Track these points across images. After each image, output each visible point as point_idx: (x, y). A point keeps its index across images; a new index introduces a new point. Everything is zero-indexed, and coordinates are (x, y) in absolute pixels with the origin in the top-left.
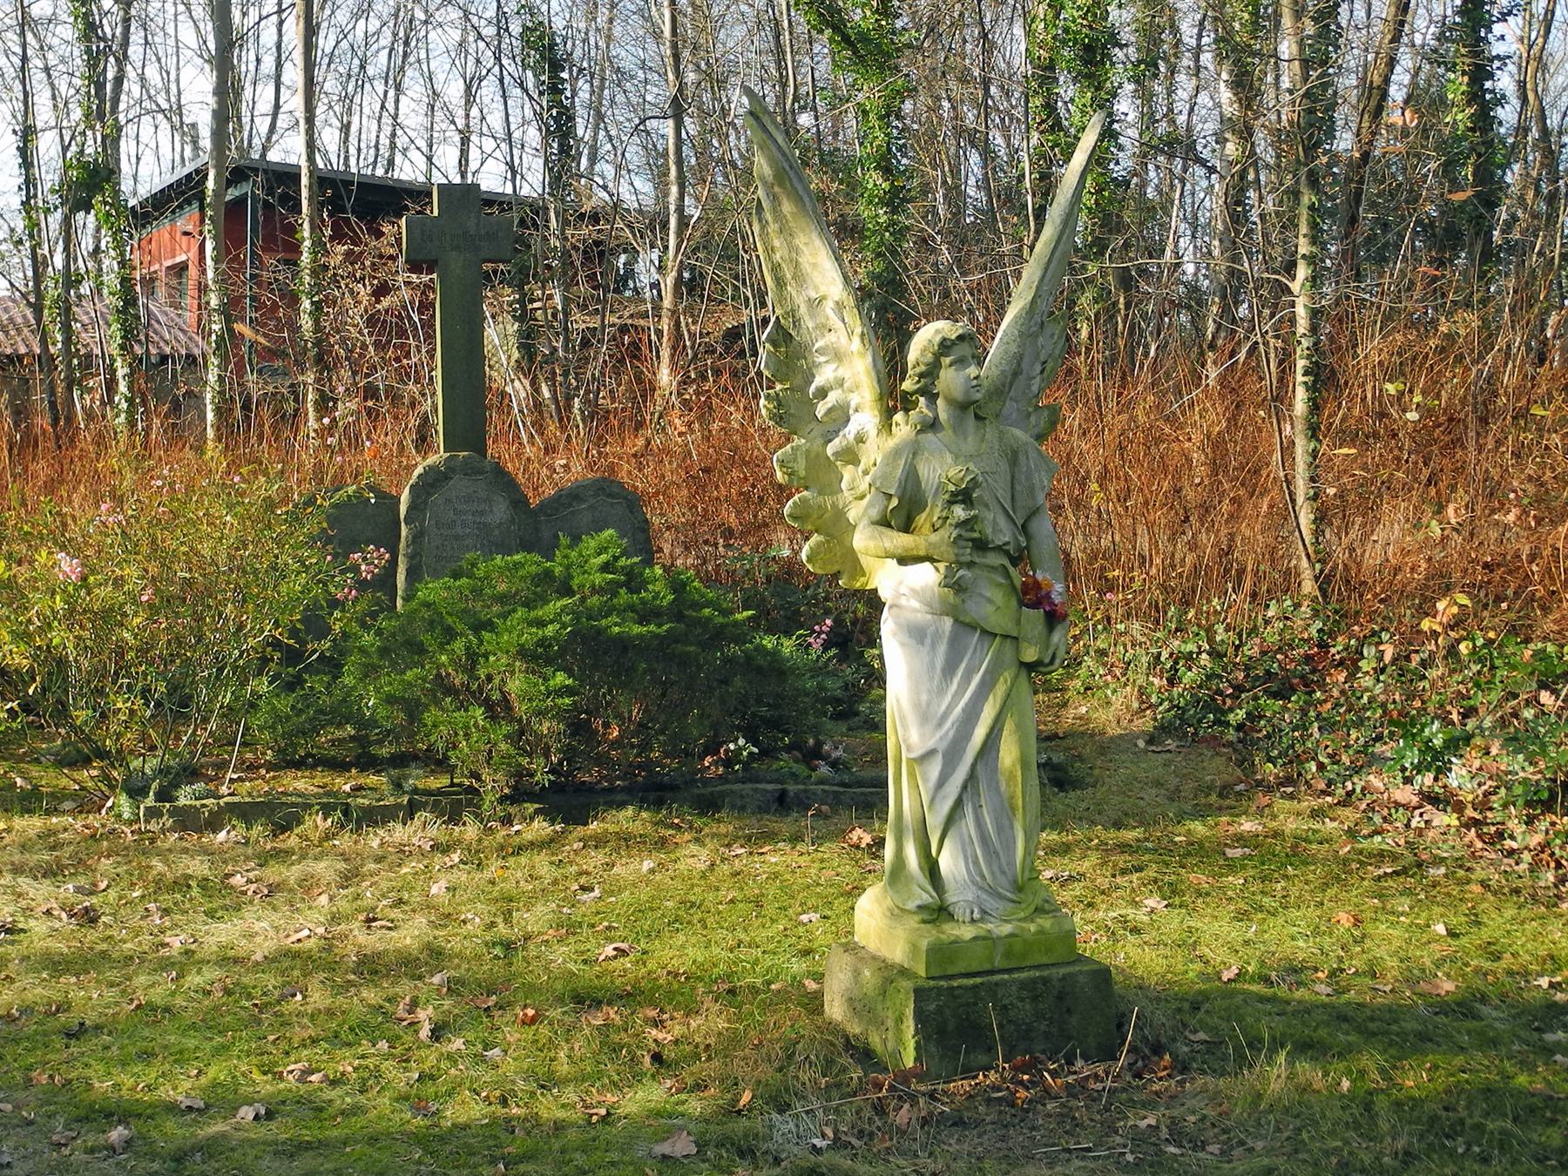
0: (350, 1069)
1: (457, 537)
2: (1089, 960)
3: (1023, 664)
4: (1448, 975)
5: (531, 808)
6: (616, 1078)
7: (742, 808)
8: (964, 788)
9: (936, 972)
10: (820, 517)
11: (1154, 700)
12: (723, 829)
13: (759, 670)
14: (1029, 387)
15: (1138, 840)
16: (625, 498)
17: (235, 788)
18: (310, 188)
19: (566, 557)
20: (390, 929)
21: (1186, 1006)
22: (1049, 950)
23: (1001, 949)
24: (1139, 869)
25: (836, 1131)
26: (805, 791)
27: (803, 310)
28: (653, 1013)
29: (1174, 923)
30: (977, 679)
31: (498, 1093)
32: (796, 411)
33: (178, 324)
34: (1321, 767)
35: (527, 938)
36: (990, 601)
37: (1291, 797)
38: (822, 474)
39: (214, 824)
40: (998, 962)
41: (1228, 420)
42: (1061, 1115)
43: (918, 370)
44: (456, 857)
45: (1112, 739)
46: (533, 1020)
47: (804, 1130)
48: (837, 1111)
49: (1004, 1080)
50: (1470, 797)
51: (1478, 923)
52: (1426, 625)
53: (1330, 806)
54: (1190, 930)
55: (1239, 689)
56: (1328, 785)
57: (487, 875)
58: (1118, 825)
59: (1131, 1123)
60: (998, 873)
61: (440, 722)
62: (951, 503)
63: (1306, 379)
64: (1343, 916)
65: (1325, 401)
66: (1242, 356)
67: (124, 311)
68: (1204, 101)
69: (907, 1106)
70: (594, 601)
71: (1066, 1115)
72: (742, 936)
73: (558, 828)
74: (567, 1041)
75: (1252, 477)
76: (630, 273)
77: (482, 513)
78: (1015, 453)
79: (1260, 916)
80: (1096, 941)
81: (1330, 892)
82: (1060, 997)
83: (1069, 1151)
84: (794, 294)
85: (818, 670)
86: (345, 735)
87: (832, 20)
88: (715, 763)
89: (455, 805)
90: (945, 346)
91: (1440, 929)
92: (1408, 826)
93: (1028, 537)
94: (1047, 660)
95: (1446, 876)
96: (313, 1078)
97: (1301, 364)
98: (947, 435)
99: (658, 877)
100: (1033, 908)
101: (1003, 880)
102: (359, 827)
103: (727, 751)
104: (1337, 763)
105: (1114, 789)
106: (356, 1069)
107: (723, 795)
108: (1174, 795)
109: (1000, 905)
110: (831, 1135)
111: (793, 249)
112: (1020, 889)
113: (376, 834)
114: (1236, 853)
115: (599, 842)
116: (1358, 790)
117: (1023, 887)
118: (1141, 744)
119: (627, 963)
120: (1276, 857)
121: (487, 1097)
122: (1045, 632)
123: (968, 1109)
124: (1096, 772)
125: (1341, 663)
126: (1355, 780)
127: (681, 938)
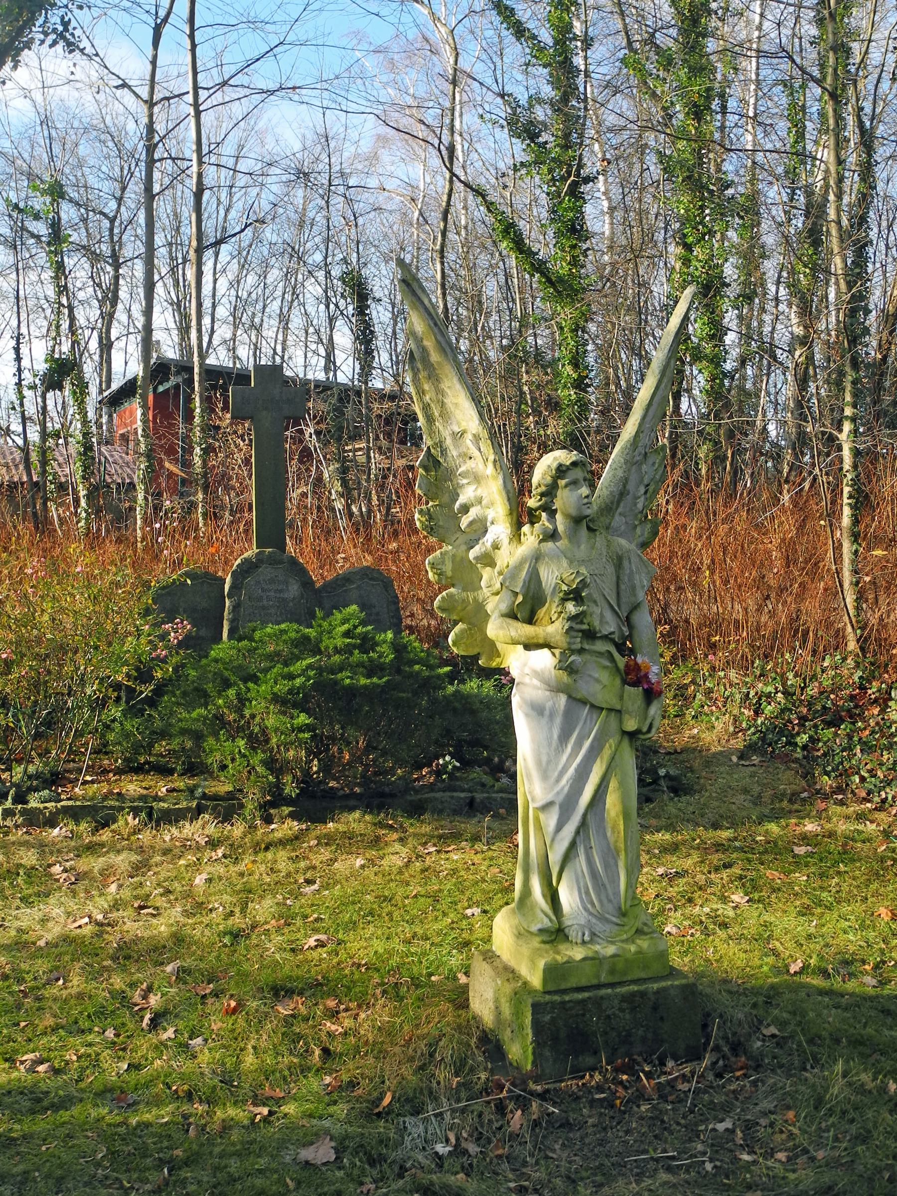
1: (264, 608)
3: (624, 733)
5: (286, 810)
7: (441, 812)
8: (577, 832)
9: (550, 988)
11: (744, 725)
12: (426, 829)
14: (635, 505)
17: (87, 790)
18: (200, 374)
19: (320, 626)
20: (154, 916)
22: (646, 967)
23: (606, 967)
24: (727, 866)
26: (488, 798)
27: (449, 442)
28: (331, 1003)
29: (753, 917)
30: (587, 744)
31: (186, 1087)
32: (446, 521)
33: (126, 465)
34: (863, 779)
36: (598, 681)
37: (842, 803)
38: (465, 575)
39: (52, 823)
40: (604, 978)
41: (797, 529)
43: (539, 490)
44: (220, 853)
45: (715, 755)
46: (234, 1011)
47: (431, 1137)
49: (606, 1080)
53: (870, 811)
55: (803, 719)
56: (868, 794)
57: (241, 867)
58: (716, 826)
59: (710, 1126)
60: (605, 901)
61: (217, 750)
62: (564, 600)
63: (850, 501)
64: (883, 911)
65: (862, 516)
66: (807, 485)
67: (85, 454)
68: (786, 325)
70: (337, 658)
75: (814, 567)
77: (281, 591)
78: (620, 559)
80: (692, 935)
81: (874, 886)
82: (655, 1008)
84: (441, 428)
88: (430, 773)
89: (227, 808)
90: (561, 471)
93: (630, 627)
94: (645, 729)
97: (847, 490)
98: (563, 543)
100: (634, 929)
101: (610, 907)
102: (158, 825)
103: (438, 765)
104: (875, 776)
107: (427, 800)
109: (608, 927)
110: (453, 1140)
111: (440, 392)
113: (169, 831)
114: (800, 850)
115: (327, 840)
116: (890, 798)
117: (627, 914)
118: (735, 759)
119: (323, 953)
121: (176, 1091)
122: (643, 705)
123: (573, 1110)
124: (702, 781)
125: (876, 701)
126: (888, 790)
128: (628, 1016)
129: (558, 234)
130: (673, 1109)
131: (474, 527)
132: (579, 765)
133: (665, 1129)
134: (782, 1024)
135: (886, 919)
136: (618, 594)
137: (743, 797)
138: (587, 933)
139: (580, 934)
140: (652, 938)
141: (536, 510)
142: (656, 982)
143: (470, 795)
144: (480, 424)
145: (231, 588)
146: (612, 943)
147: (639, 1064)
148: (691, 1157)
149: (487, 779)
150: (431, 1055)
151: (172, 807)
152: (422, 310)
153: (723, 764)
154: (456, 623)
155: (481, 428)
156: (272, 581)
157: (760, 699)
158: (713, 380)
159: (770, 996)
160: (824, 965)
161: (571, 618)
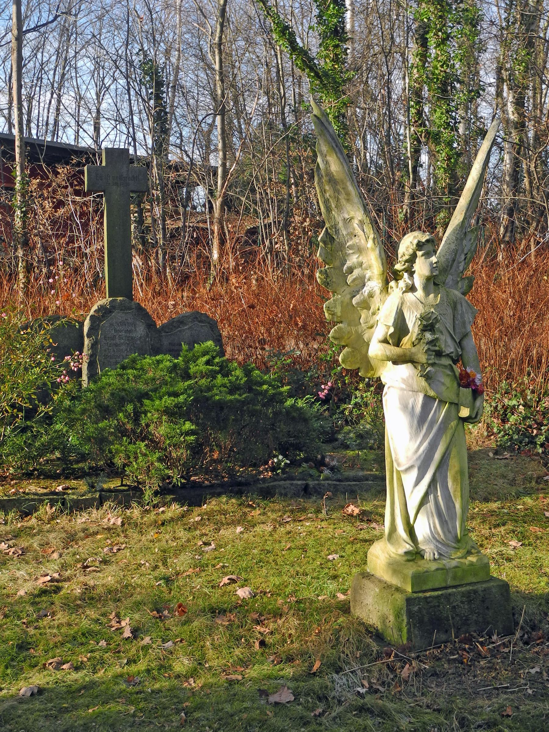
0: (85, 659)
1: (116, 345)
5: (169, 498)
6: (241, 656)
8: (429, 486)
10: (349, 338)
11: (495, 430)
13: (293, 418)
14: (458, 267)
15: (499, 508)
16: (209, 323)
18: (21, 147)
22: (475, 575)
23: (451, 575)
25: (370, 683)
26: (319, 484)
27: (341, 225)
29: (527, 555)
35: (178, 574)
36: (443, 384)
38: (351, 314)
40: (450, 582)
42: (488, 668)
43: (405, 258)
45: (475, 452)
48: (369, 671)
54: (537, 558)
59: (527, 671)
60: (447, 532)
69: (407, 666)
72: (298, 569)
73: (185, 508)
74: (210, 635)
76: (189, 198)
77: (130, 331)
83: (497, 689)
84: (336, 215)
86: (54, 457)
89: (130, 495)
94: (474, 416)
96: (64, 667)
99: (246, 536)
101: (450, 536)
102: (72, 512)
105: (481, 480)
106: (89, 659)
107: (274, 487)
108: (513, 482)
118: (491, 455)
123: (438, 666)
128: (466, 607)
129: (324, 36)
130: (501, 662)
131: (356, 282)
132: (431, 441)
139: (432, 554)
141: (400, 272)
143: (304, 482)
145: (90, 329)
147: (474, 638)
148: (518, 687)
149: (314, 472)
150: (337, 639)
151: (80, 498)
153: (483, 458)
154: (344, 347)
155: (365, 216)
156: (123, 323)
157: (506, 411)
158: (449, 159)
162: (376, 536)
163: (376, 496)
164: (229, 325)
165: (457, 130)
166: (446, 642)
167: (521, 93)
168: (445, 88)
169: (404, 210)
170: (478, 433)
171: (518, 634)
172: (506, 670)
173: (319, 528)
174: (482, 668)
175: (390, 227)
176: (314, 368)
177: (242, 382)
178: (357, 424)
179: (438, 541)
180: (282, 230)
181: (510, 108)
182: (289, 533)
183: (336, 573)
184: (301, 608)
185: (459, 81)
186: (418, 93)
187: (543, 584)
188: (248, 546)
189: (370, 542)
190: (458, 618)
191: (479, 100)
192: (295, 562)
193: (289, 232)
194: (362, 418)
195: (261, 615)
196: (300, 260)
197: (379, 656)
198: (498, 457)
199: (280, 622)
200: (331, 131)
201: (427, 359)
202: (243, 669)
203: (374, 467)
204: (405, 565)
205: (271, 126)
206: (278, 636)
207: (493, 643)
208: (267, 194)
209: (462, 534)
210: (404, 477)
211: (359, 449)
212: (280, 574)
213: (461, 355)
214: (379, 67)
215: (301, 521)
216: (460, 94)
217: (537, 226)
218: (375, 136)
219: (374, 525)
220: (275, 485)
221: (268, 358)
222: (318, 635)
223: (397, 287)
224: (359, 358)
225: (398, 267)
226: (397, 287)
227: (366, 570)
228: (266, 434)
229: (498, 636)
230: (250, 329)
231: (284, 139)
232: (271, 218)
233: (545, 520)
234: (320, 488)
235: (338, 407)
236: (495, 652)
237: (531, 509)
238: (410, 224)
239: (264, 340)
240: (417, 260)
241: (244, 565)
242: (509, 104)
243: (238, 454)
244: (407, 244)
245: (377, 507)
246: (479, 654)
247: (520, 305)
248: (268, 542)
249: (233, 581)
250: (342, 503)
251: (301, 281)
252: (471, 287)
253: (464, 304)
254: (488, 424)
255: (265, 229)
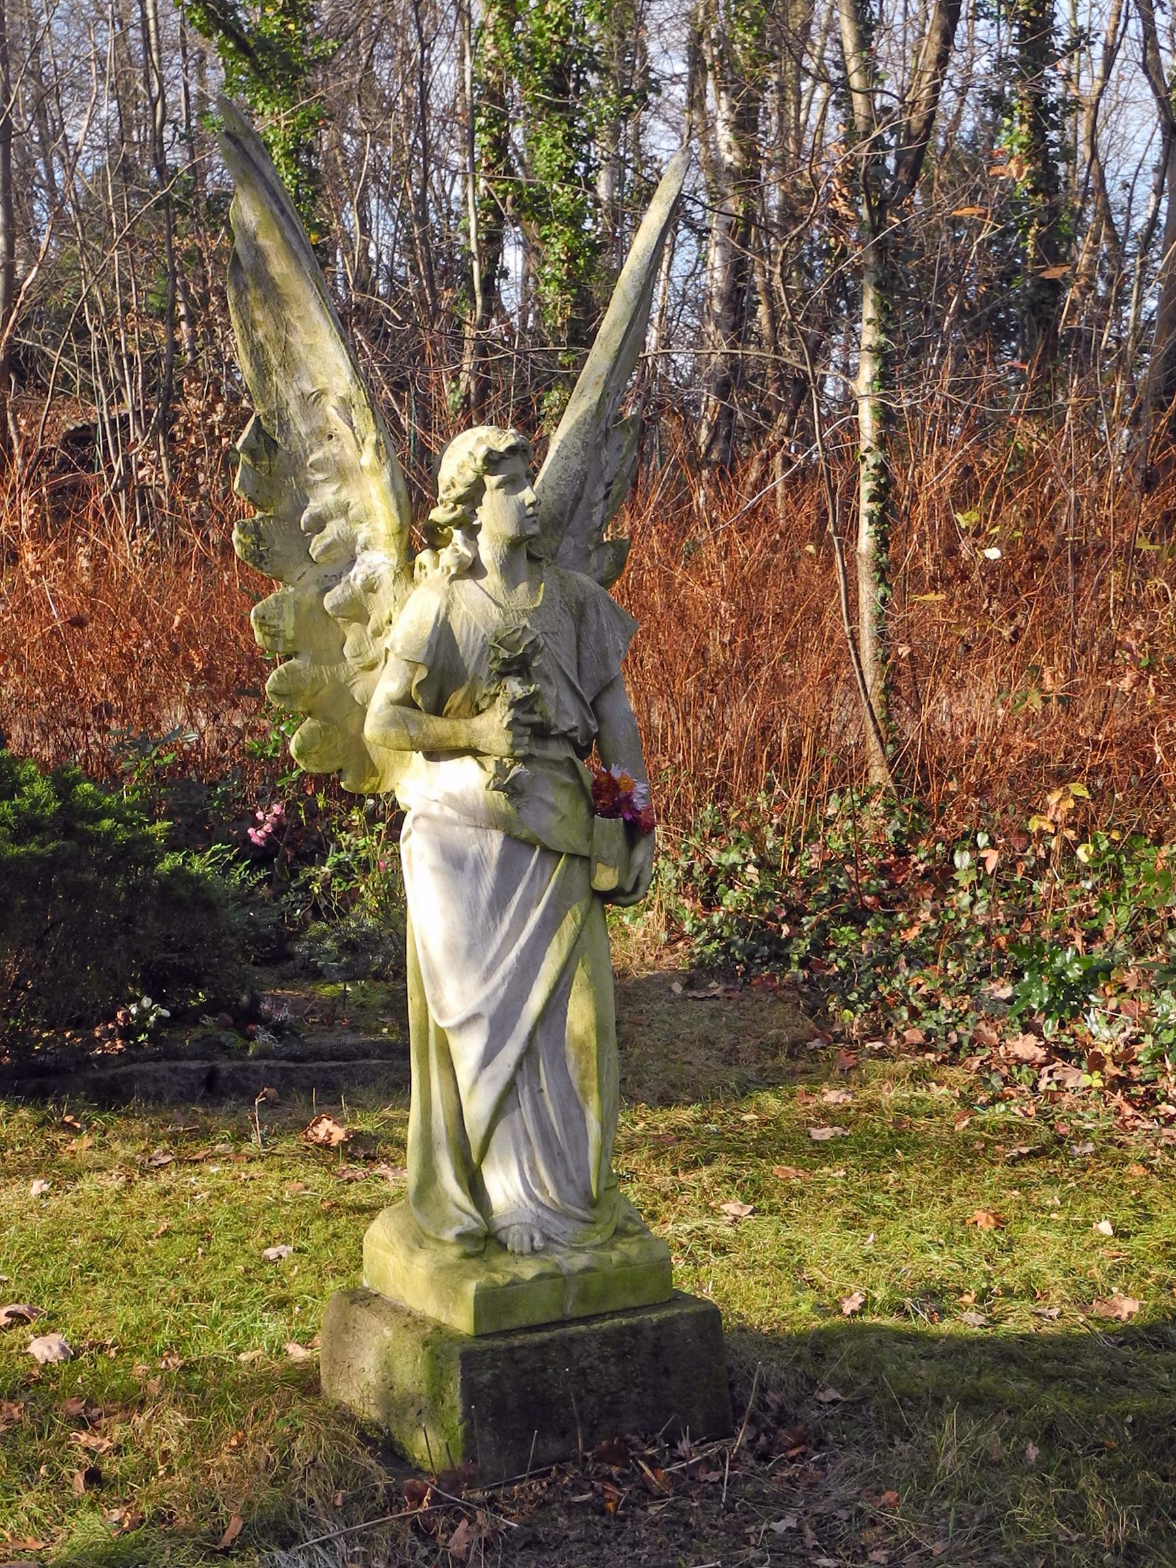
2: (691, 1299)
4: (1125, 1290)
6: (38, 1512)
8: (519, 1065)
11: (688, 927)
12: (136, 1129)
14: (590, 516)
15: (697, 1122)
21: (806, 1352)
23: (574, 1290)
26: (244, 1069)
27: (293, 408)
29: (766, 1235)
34: (915, 1014)
36: (553, 808)
37: (881, 1055)
38: (321, 632)
42: (670, 1522)
45: (638, 983)
48: (367, 1540)
50: (1108, 1049)
51: (1149, 1218)
52: (1034, 825)
53: (933, 1066)
58: (666, 1101)
59: (764, 1527)
60: (564, 1183)
62: (502, 674)
64: (980, 1216)
69: (464, 1524)
71: (678, 1522)
72: (189, 1284)
79: (875, 1220)
81: (958, 1182)
82: (656, 1354)
84: (281, 386)
85: (246, 898)
87: (218, 17)
91: (1105, 1228)
92: (1034, 1088)
93: (600, 720)
94: (629, 888)
95: (1096, 1155)
99: (54, 1203)
100: (611, 1228)
103: (127, 1015)
107: (129, 1078)
108: (731, 1057)
111: (283, 325)
112: (592, 1203)
116: (966, 1044)
118: (677, 988)
120: (883, 1144)
123: (543, 1522)
127: (101, 1290)
128: (613, 1370)
130: (702, 1506)
131: (334, 554)
132: (522, 951)
133: (694, 1536)
134: (846, 1386)
135: (987, 1228)
136: (579, 665)
137: (703, 1053)
138: (537, 1237)
139: (526, 1238)
140: (641, 1240)
141: (443, 527)
142: (654, 1311)
143: (206, 1064)
144: (354, 380)
146: (580, 1250)
147: (633, 1447)
149: (231, 1038)
150: (285, 1461)
152: (261, 187)
153: (659, 997)
155: (354, 388)
157: (713, 878)
158: (572, 259)
159: (819, 1346)
160: (898, 1298)
161: (516, 704)
162: (387, 1197)
163: (389, 1096)
164: (19, 670)
165: (591, 186)
166: (561, 1462)
167: (750, 98)
168: (559, 83)
169: (463, 385)
170: (645, 935)
171: (741, 1438)
172: (712, 1527)
173: (243, 1179)
174: (655, 1524)
175: (426, 427)
176: (234, 777)
177: (48, 812)
178: (342, 916)
179: (540, 1205)
180: (154, 434)
181: (724, 135)
182: (166, 1193)
183: (284, 1292)
184: (197, 1387)
185: (595, 68)
186: (495, 95)
187: (804, 1308)
188: (59, 1233)
189: (368, 1211)
190: (592, 1400)
191: (645, 115)
192: (179, 1267)
193: (172, 437)
194: (354, 902)
195: (91, 1404)
196: (199, 508)
197: (393, 1500)
198: (695, 993)
199: (140, 1421)
200: (268, 172)
201: (513, 746)
202: (42, 1545)
203: (384, 1025)
204: (459, 1267)
205: (126, 171)
206: (133, 1458)
207: (681, 1459)
208: (117, 343)
209: (603, 1184)
210: (454, 1043)
211: (346, 980)
212: (141, 1298)
213: (597, 736)
214: (401, 31)
215: (196, 1161)
216: (597, 93)
217: (791, 422)
218: (388, 200)
219: (382, 1169)
220: (131, 1074)
221: (116, 750)
222: (235, 1451)
223: (436, 565)
224: (340, 745)
225: (438, 514)
226: (436, 565)
227: (361, 1284)
228: (110, 943)
229: (692, 1440)
230: (71, 680)
231: (158, 205)
232: (129, 403)
233: (810, 1148)
234: (247, 1078)
235: (295, 875)
236: (684, 1484)
237: (776, 1122)
238: (475, 411)
239: (108, 707)
240: (487, 498)
241: (49, 1278)
242: (719, 125)
243: (38, 994)
244: (462, 455)
245: (390, 1123)
246: (645, 1489)
247: (749, 618)
248: (112, 1218)
249: (19, 1319)
250: (304, 1116)
251: (204, 561)
252: (622, 565)
253: (604, 608)
254: (669, 912)
255: (113, 431)
